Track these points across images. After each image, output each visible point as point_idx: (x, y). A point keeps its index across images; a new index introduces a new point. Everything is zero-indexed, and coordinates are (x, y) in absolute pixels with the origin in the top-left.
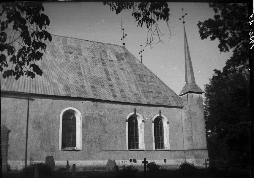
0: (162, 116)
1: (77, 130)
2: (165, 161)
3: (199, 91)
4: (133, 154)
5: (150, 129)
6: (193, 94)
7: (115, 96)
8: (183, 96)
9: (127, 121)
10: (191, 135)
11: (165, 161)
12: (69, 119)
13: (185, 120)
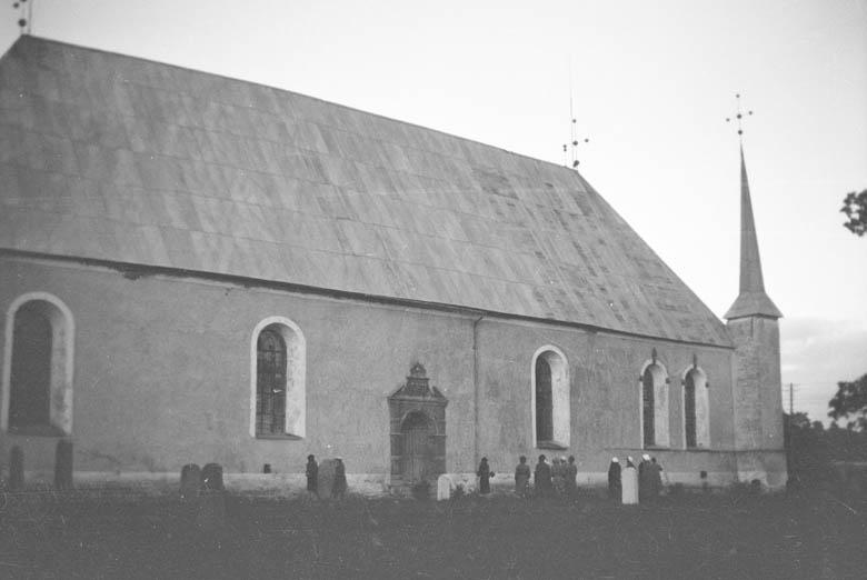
0: (699, 368)
1: (554, 404)
2: (704, 475)
3: (769, 312)
4: (268, 449)
5: (678, 400)
6: (766, 321)
7: (390, 267)
8: (736, 321)
9: (641, 379)
10: (757, 417)
11: (704, 475)
12: (273, 341)
13: (740, 380)
